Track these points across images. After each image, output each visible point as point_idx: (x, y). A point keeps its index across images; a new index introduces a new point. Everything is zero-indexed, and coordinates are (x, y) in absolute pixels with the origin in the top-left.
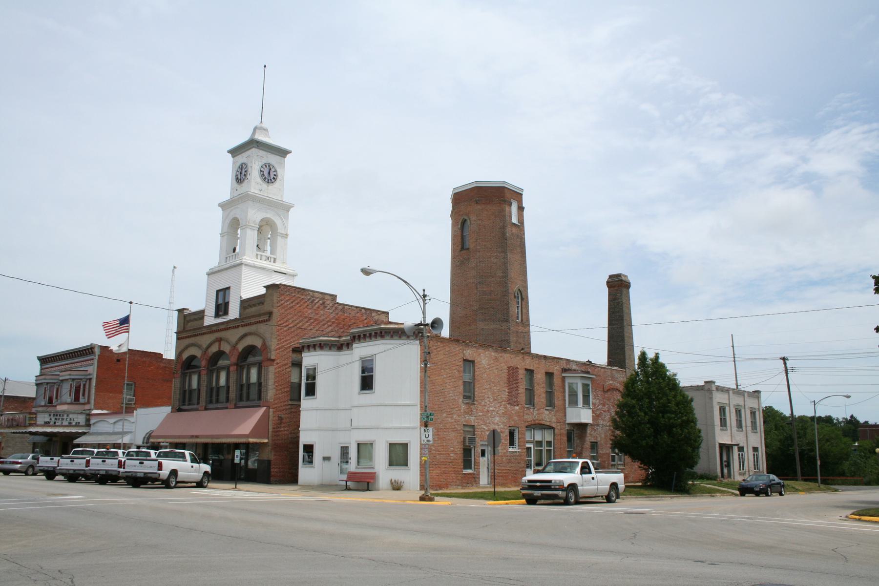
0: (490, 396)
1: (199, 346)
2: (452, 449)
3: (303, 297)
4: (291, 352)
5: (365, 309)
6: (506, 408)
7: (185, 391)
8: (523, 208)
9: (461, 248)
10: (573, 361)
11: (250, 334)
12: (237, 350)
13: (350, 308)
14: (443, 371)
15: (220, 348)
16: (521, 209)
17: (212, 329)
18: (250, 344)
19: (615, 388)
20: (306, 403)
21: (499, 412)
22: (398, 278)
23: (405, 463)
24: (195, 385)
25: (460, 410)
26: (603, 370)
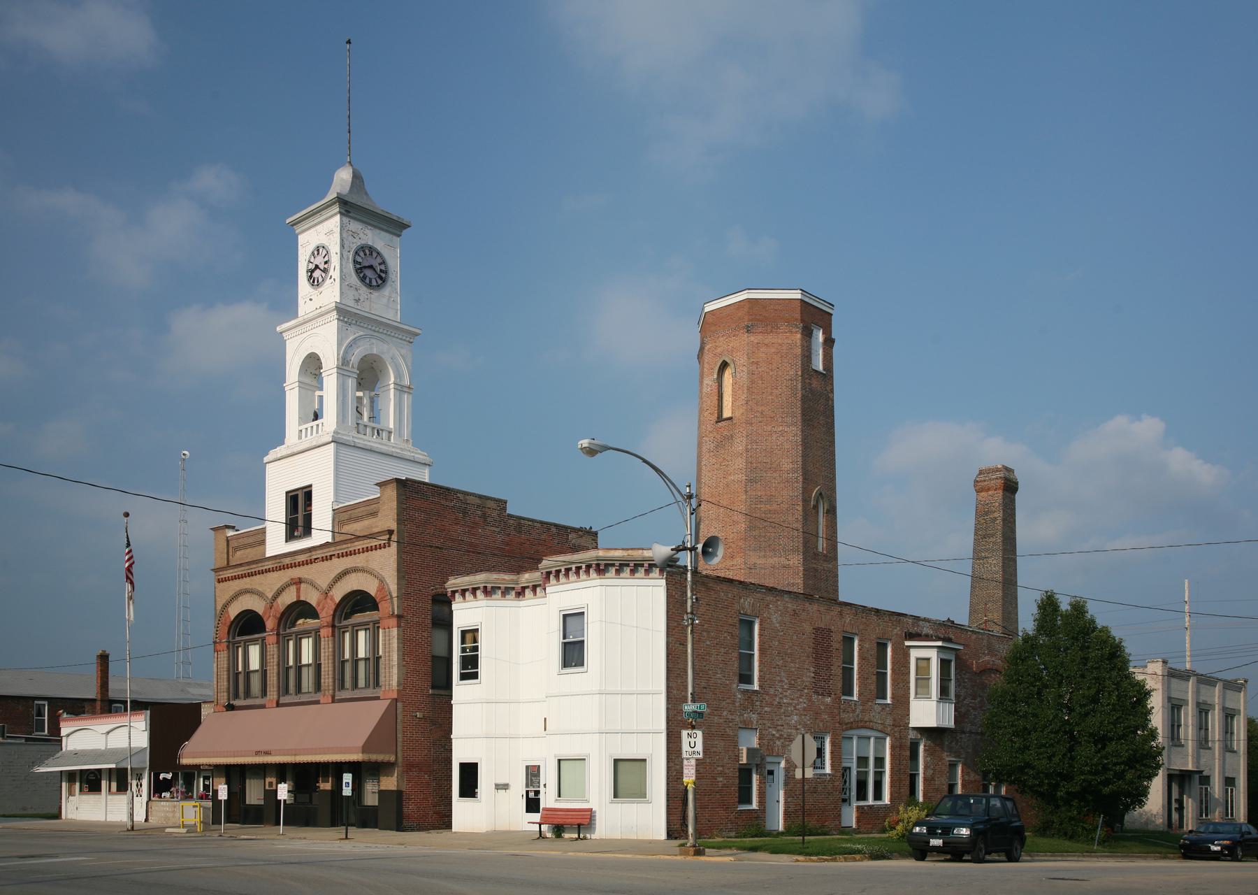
0: (784, 679)
1: (260, 595)
2: (720, 769)
3: (447, 503)
4: (430, 602)
5: (556, 526)
6: (810, 700)
7: (237, 674)
8: (833, 341)
9: (718, 418)
10: (925, 620)
11: (355, 570)
12: (332, 599)
13: (530, 523)
14: (705, 634)
15: (298, 596)
16: (829, 342)
17: (282, 563)
18: (355, 589)
19: (995, 667)
20: (461, 691)
21: (797, 707)
22: (645, 461)
23: (640, 793)
24: (255, 664)
25: (734, 703)
26: (974, 637)
